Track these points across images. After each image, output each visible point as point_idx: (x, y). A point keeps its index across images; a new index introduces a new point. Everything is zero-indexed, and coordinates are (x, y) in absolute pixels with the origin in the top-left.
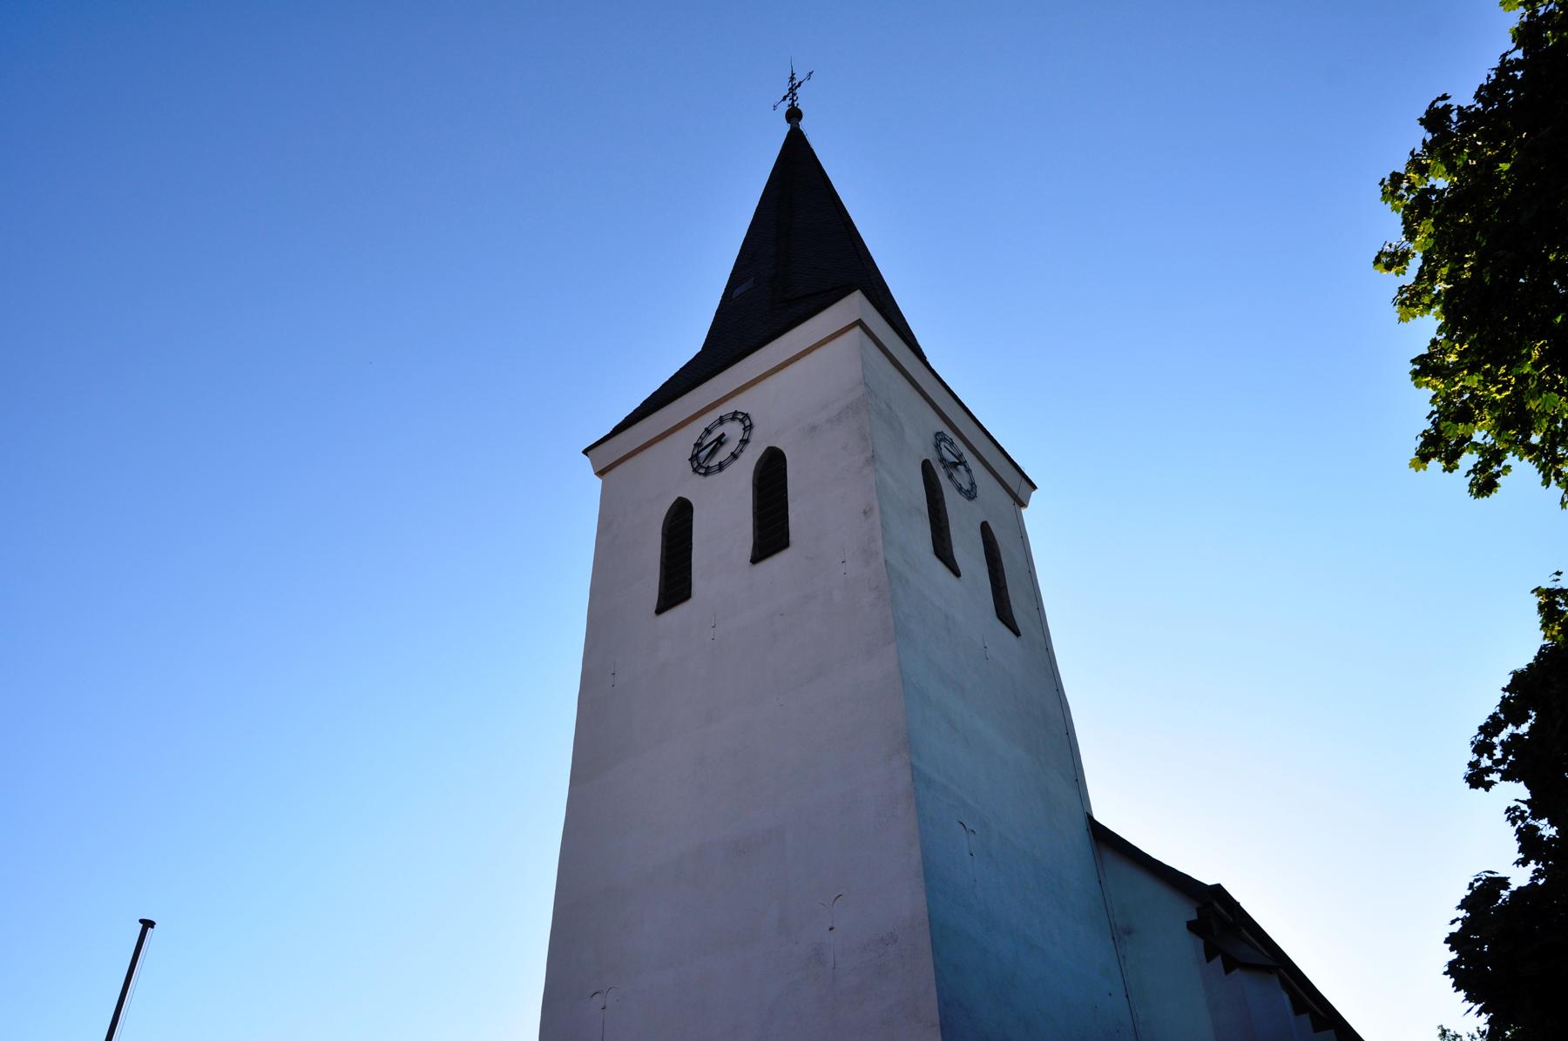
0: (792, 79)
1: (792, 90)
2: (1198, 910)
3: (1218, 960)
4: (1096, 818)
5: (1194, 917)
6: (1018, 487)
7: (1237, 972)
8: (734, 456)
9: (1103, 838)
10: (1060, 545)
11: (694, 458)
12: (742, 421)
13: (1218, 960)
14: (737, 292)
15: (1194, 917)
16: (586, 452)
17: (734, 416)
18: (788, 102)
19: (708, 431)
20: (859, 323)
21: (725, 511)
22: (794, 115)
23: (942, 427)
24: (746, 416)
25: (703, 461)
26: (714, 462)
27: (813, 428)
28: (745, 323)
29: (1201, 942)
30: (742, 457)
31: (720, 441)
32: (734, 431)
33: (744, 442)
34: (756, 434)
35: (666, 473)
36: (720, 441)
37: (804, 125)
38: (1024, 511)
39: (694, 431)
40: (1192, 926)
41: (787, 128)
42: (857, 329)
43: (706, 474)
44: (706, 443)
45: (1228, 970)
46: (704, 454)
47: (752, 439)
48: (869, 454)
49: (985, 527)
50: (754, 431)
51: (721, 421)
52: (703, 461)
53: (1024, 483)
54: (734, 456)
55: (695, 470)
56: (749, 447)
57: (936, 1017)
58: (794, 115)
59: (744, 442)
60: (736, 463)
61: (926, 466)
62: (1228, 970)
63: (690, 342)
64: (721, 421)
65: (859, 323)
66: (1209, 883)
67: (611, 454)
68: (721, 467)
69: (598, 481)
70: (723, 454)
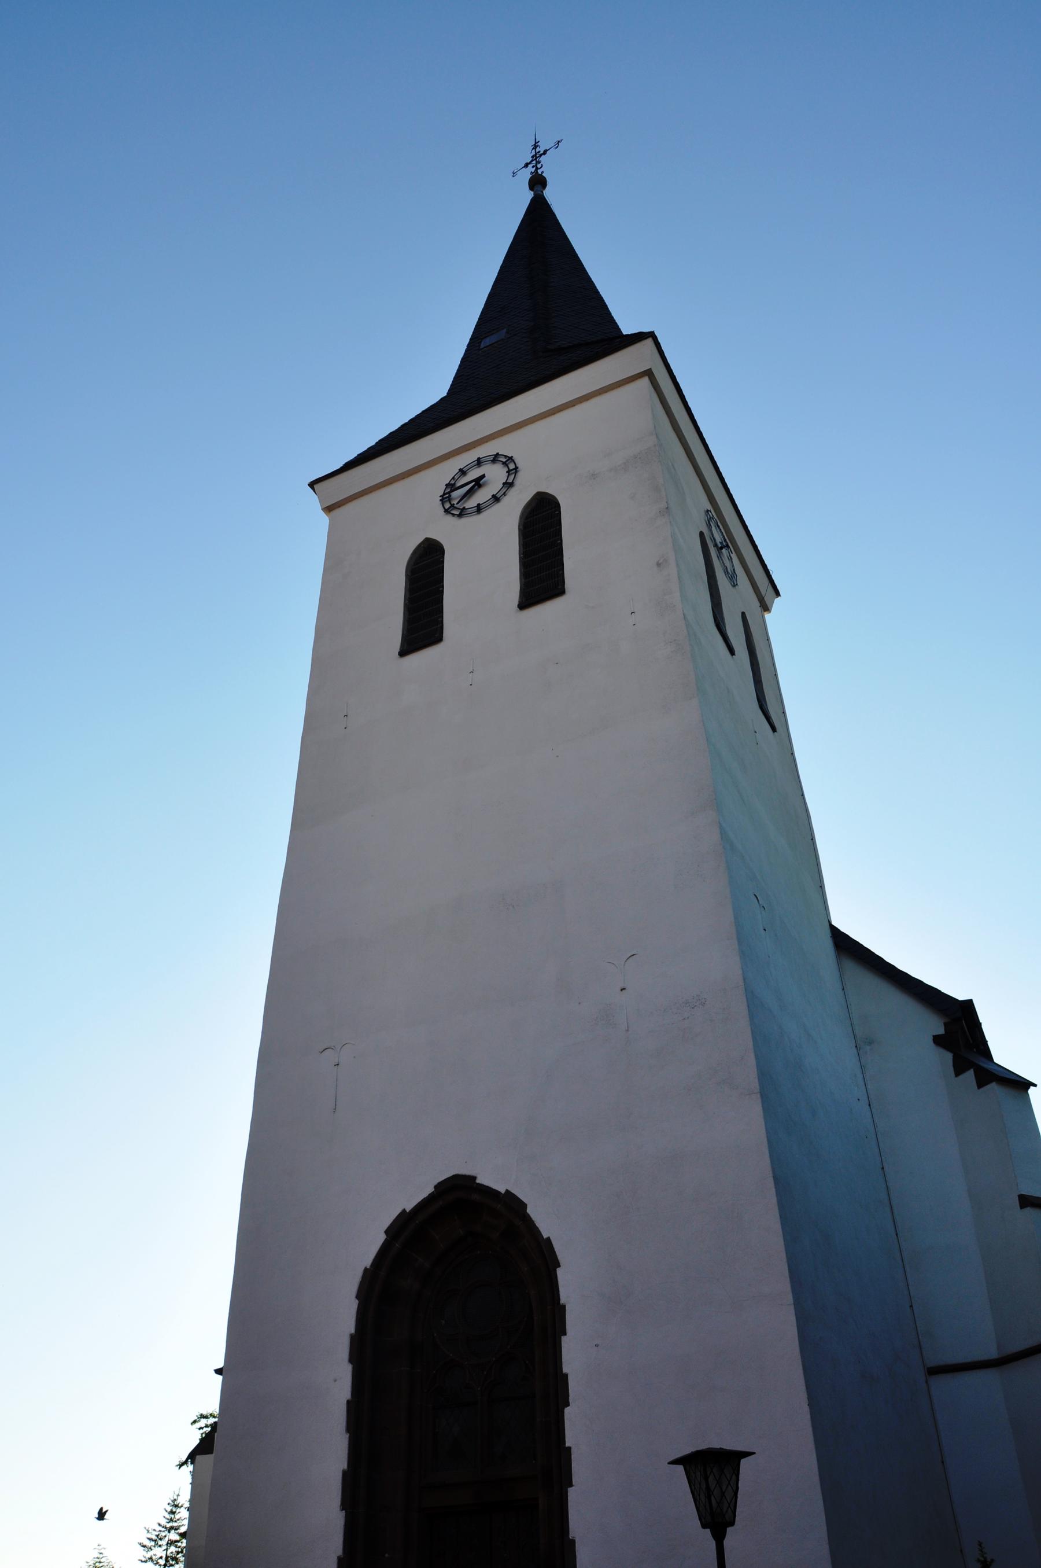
0: (535, 146)
1: (536, 158)
2: (945, 1024)
3: (970, 1075)
4: (834, 923)
5: (941, 1031)
6: (766, 592)
7: (993, 1086)
8: (496, 499)
9: (845, 945)
10: (810, 648)
11: (445, 498)
12: (504, 463)
13: (970, 1075)
14: (487, 342)
15: (941, 1031)
16: (312, 485)
17: (495, 459)
18: (531, 169)
19: (463, 472)
20: (649, 373)
21: (483, 558)
22: (538, 182)
23: (710, 508)
24: (511, 459)
25: (456, 500)
26: (471, 503)
27: (594, 476)
28: (487, 376)
29: (949, 1056)
30: (505, 501)
31: (478, 483)
32: (496, 475)
33: (508, 485)
34: (521, 479)
35: (413, 511)
36: (478, 483)
37: (549, 194)
38: (767, 616)
39: (448, 471)
40: (938, 1040)
41: (530, 195)
42: (646, 380)
43: (460, 516)
44: (458, 484)
45: (980, 1084)
46: (457, 494)
47: (517, 482)
48: (663, 505)
49: (743, 614)
50: (520, 475)
51: (479, 462)
52: (456, 500)
53: (770, 588)
54: (496, 499)
55: (447, 511)
56: (512, 492)
57: (755, 1084)
58: (538, 182)
59: (508, 485)
60: (497, 507)
61: (701, 534)
62: (980, 1084)
63: (435, 385)
64: (479, 462)
65: (649, 373)
66: (960, 998)
67: (341, 488)
68: (479, 509)
69: (324, 519)
70: (482, 496)
